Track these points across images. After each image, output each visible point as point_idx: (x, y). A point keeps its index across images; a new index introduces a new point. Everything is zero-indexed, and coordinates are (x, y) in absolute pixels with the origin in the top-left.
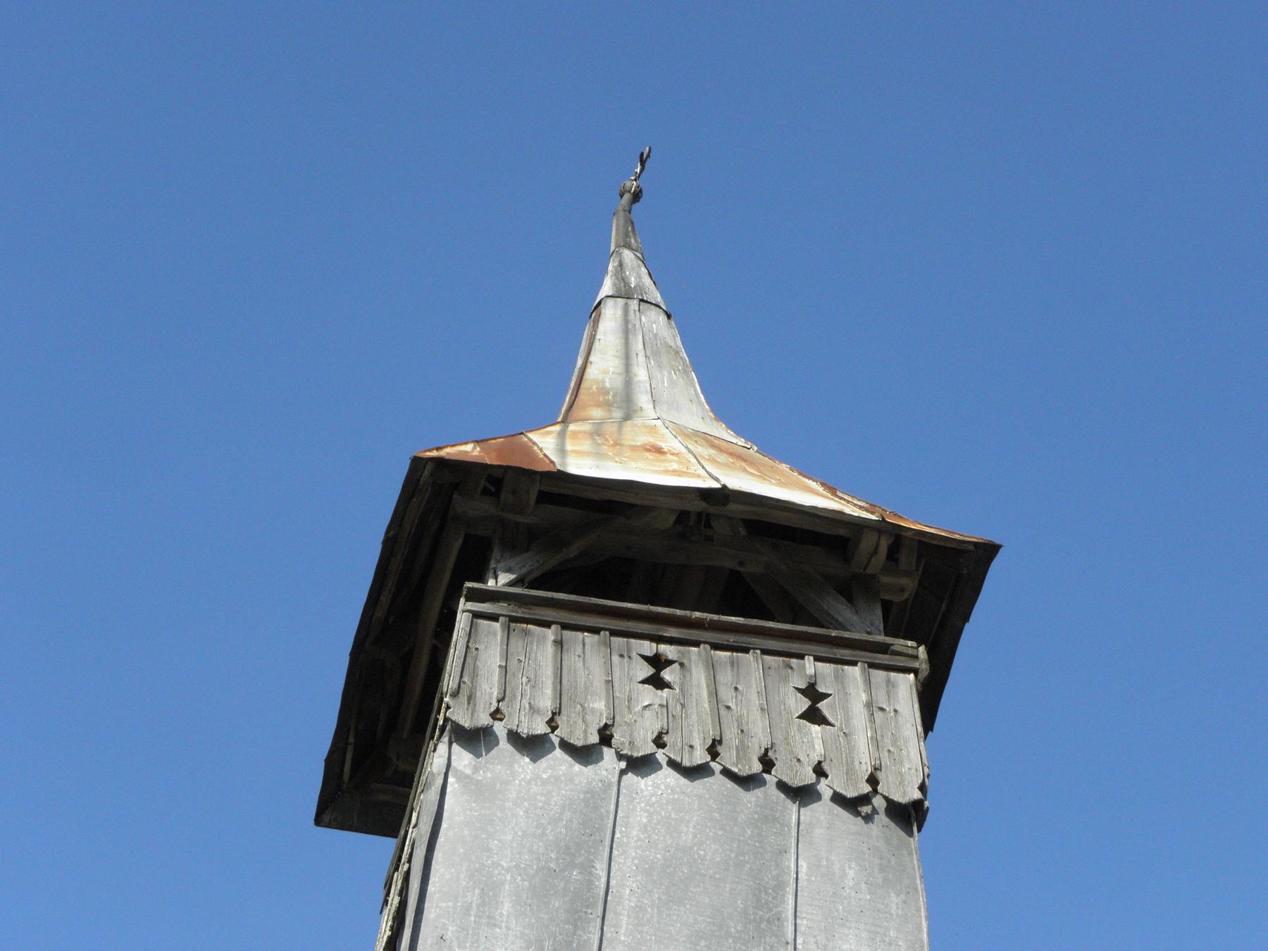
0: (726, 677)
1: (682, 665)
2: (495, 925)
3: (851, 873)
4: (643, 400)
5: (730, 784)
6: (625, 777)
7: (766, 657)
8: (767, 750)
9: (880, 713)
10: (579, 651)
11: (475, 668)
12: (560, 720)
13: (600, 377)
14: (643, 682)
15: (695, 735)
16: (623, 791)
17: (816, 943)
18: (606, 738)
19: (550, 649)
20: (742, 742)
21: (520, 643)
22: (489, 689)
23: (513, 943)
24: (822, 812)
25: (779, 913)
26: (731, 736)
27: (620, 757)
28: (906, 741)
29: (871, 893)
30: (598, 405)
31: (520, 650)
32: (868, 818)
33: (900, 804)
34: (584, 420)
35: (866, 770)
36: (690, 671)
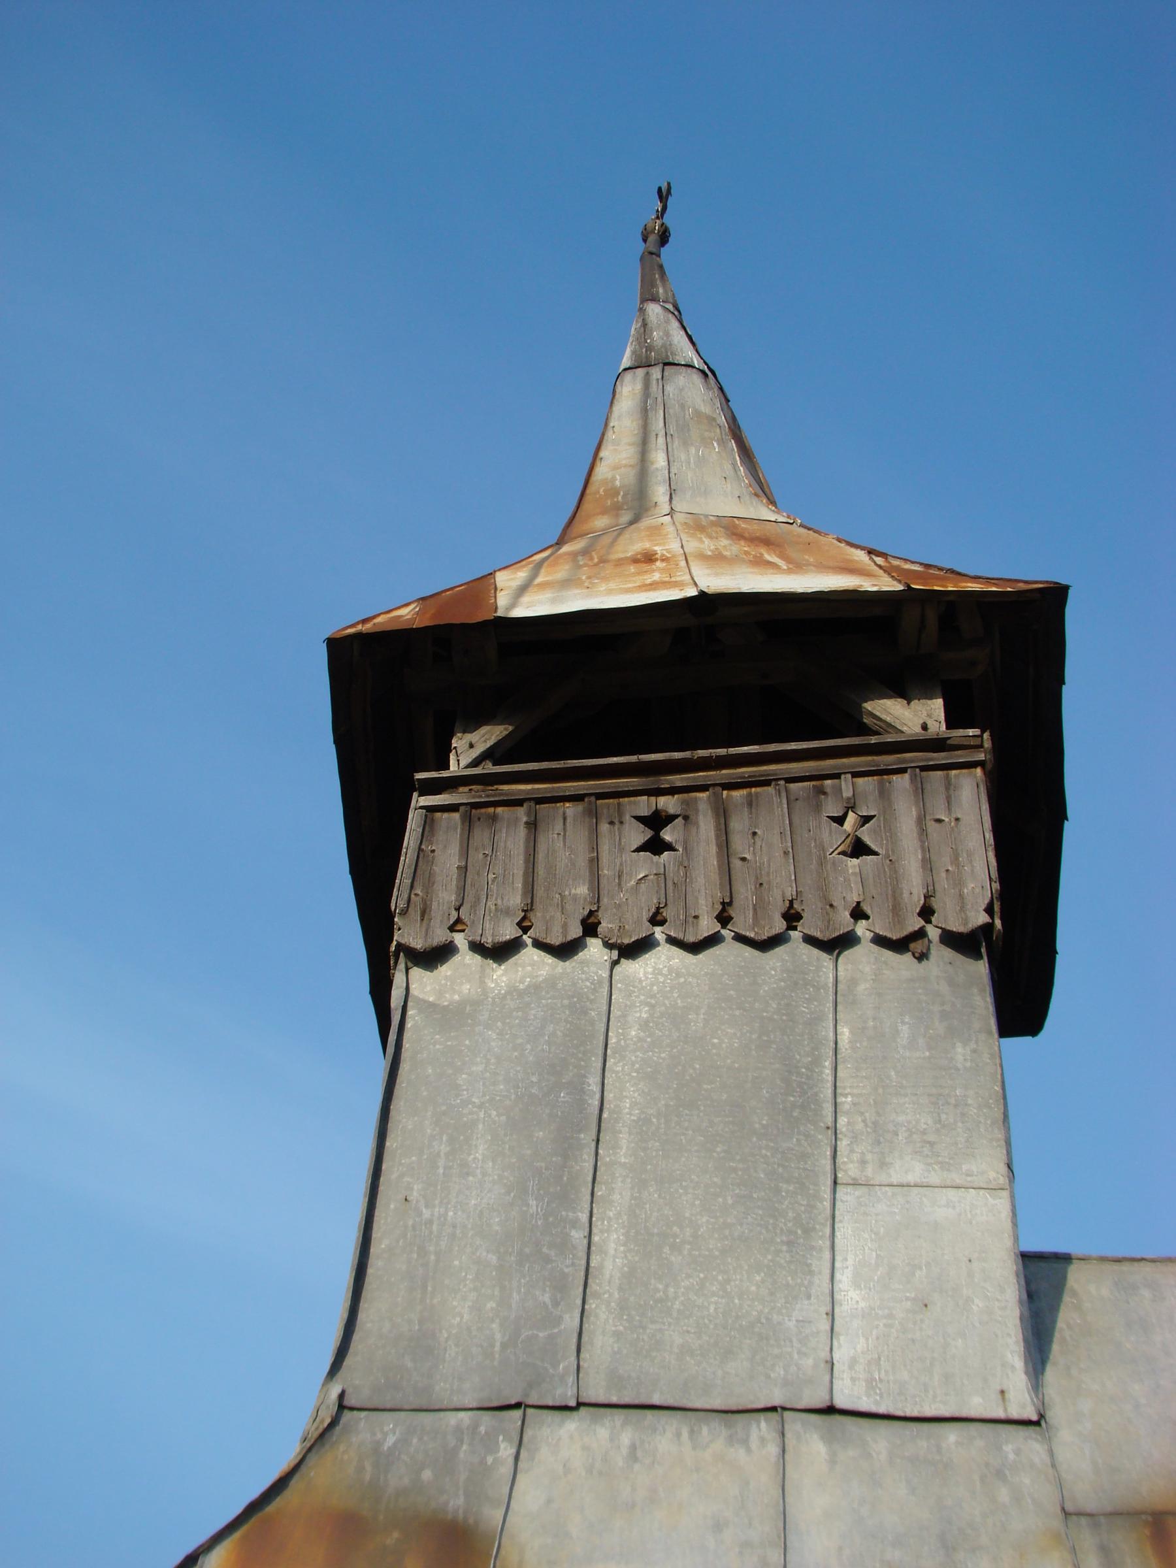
0: (739, 824)
1: (686, 818)
2: (468, 1174)
3: (905, 1030)
4: (660, 493)
5: (748, 952)
6: (617, 969)
7: (792, 786)
8: (791, 902)
9: (937, 825)
10: (559, 827)
11: (431, 875)
12: (536, 918)
13: (609, 476)
14: (638, 850)
15: (702, 901)
16: (618, 985)
17: (864, 1121)
18: (590, 928)
19: (522, 832)
20: (760, 899)
21: (486, 834)
22: (445, 897)
23: (490, 1191)
24: (863, 959)
25: (816, 1094)
26: (745, 894)
27: (609, 945)
28: (970, 854)
29: (930, 1048)
30: (604, 512)
31: (487, 841)
32: (922, 957)
33: (961, 934)
34: (581, 536)
35: (914, 897)
36: (697, 824)
